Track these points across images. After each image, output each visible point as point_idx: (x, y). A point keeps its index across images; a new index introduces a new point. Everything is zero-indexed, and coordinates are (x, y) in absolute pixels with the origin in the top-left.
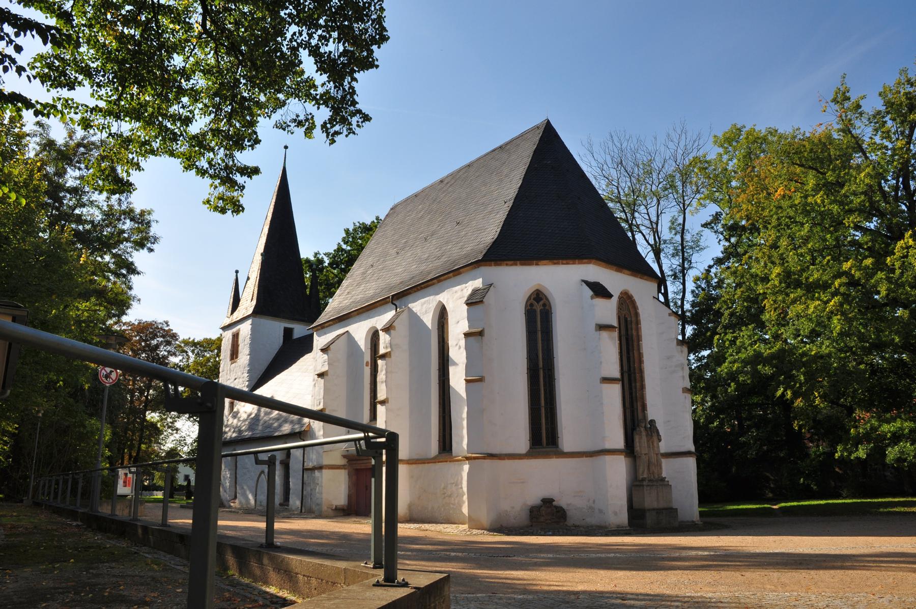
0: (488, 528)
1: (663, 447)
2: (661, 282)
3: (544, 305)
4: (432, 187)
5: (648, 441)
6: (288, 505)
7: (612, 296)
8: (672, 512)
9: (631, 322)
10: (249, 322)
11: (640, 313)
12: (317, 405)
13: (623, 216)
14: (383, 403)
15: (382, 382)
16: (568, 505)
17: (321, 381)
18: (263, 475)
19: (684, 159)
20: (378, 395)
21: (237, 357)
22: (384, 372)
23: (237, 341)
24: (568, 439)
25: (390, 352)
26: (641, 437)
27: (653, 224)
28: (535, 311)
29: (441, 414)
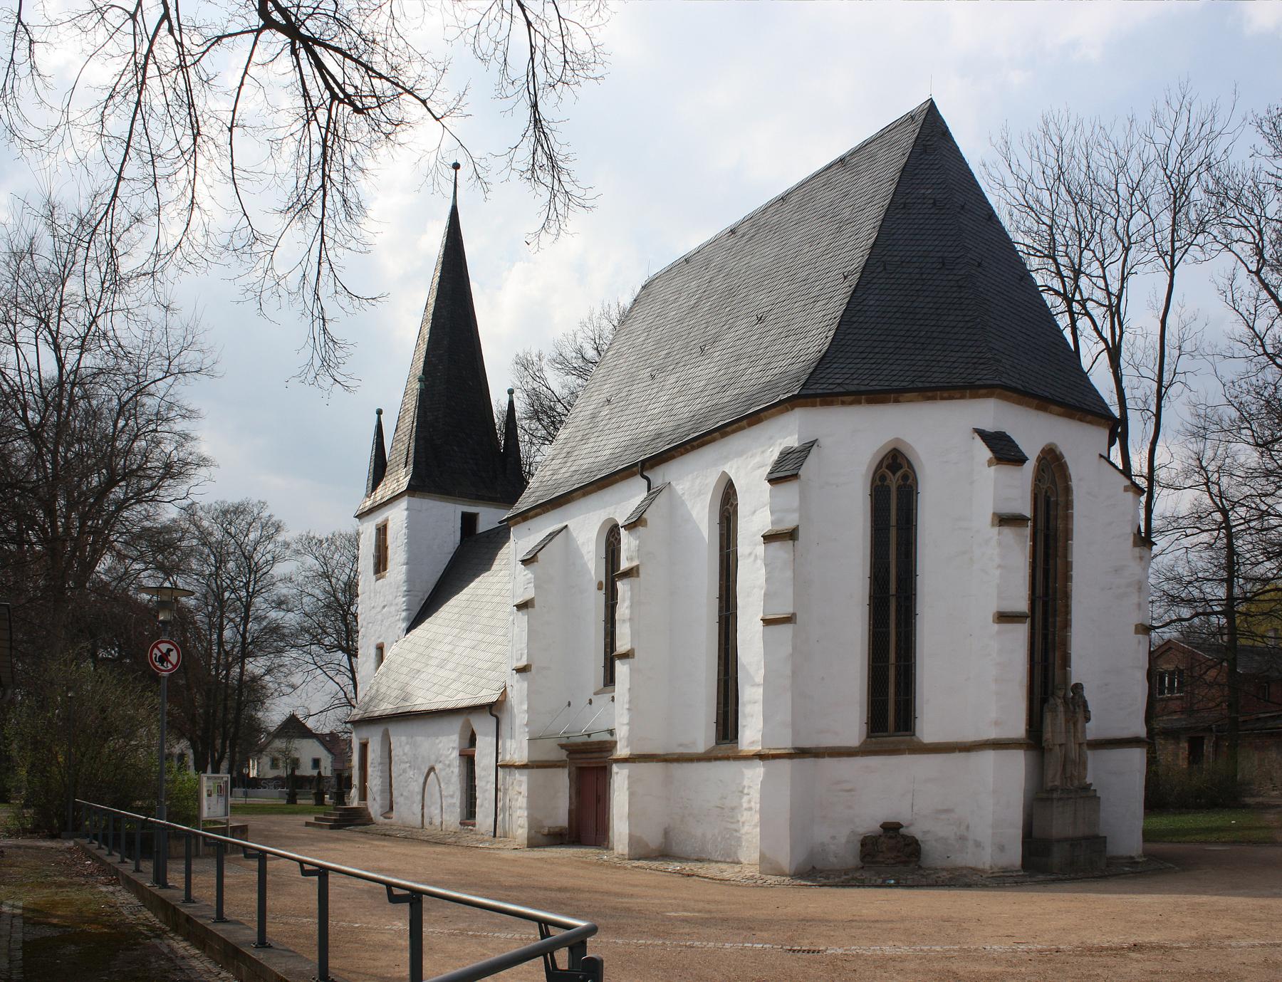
0: (792, 873)
1: (1093, 730)
2: (1117, 429)
3: (905, 477)
4: (715, 242)
5: (1067, 721)
6: (474, 825)
7: (1027, 459)
8: (1096, 842)
9: (1057, 503)
10: (403, 504)
11: (1075, 488)
12: (517, 660)
13: (1056, 284)
14: (626, 656)
15: (624, 621)
16: (925, 833)
17: (522, 618)
18: (432, 773)
19: (1182, 163)
20: (618, 644)
21: (385, 569)
22: (627, 603)
23: (385, 540)
24: (929, 727)
25: (637, 567)
26: (1057, 716)
27: (1113, 297)
28: (888, 489)
29: (722, 677)
